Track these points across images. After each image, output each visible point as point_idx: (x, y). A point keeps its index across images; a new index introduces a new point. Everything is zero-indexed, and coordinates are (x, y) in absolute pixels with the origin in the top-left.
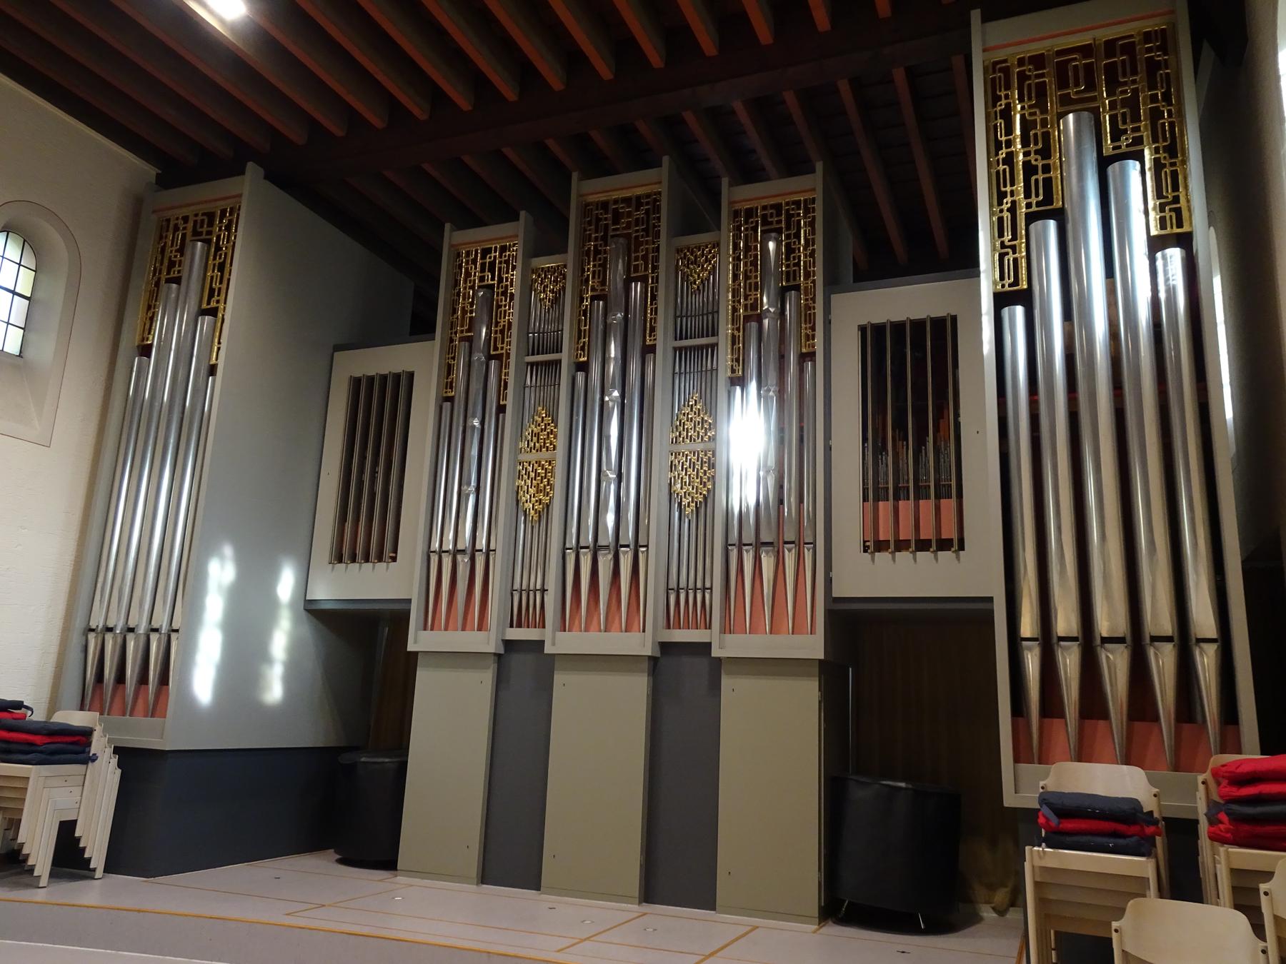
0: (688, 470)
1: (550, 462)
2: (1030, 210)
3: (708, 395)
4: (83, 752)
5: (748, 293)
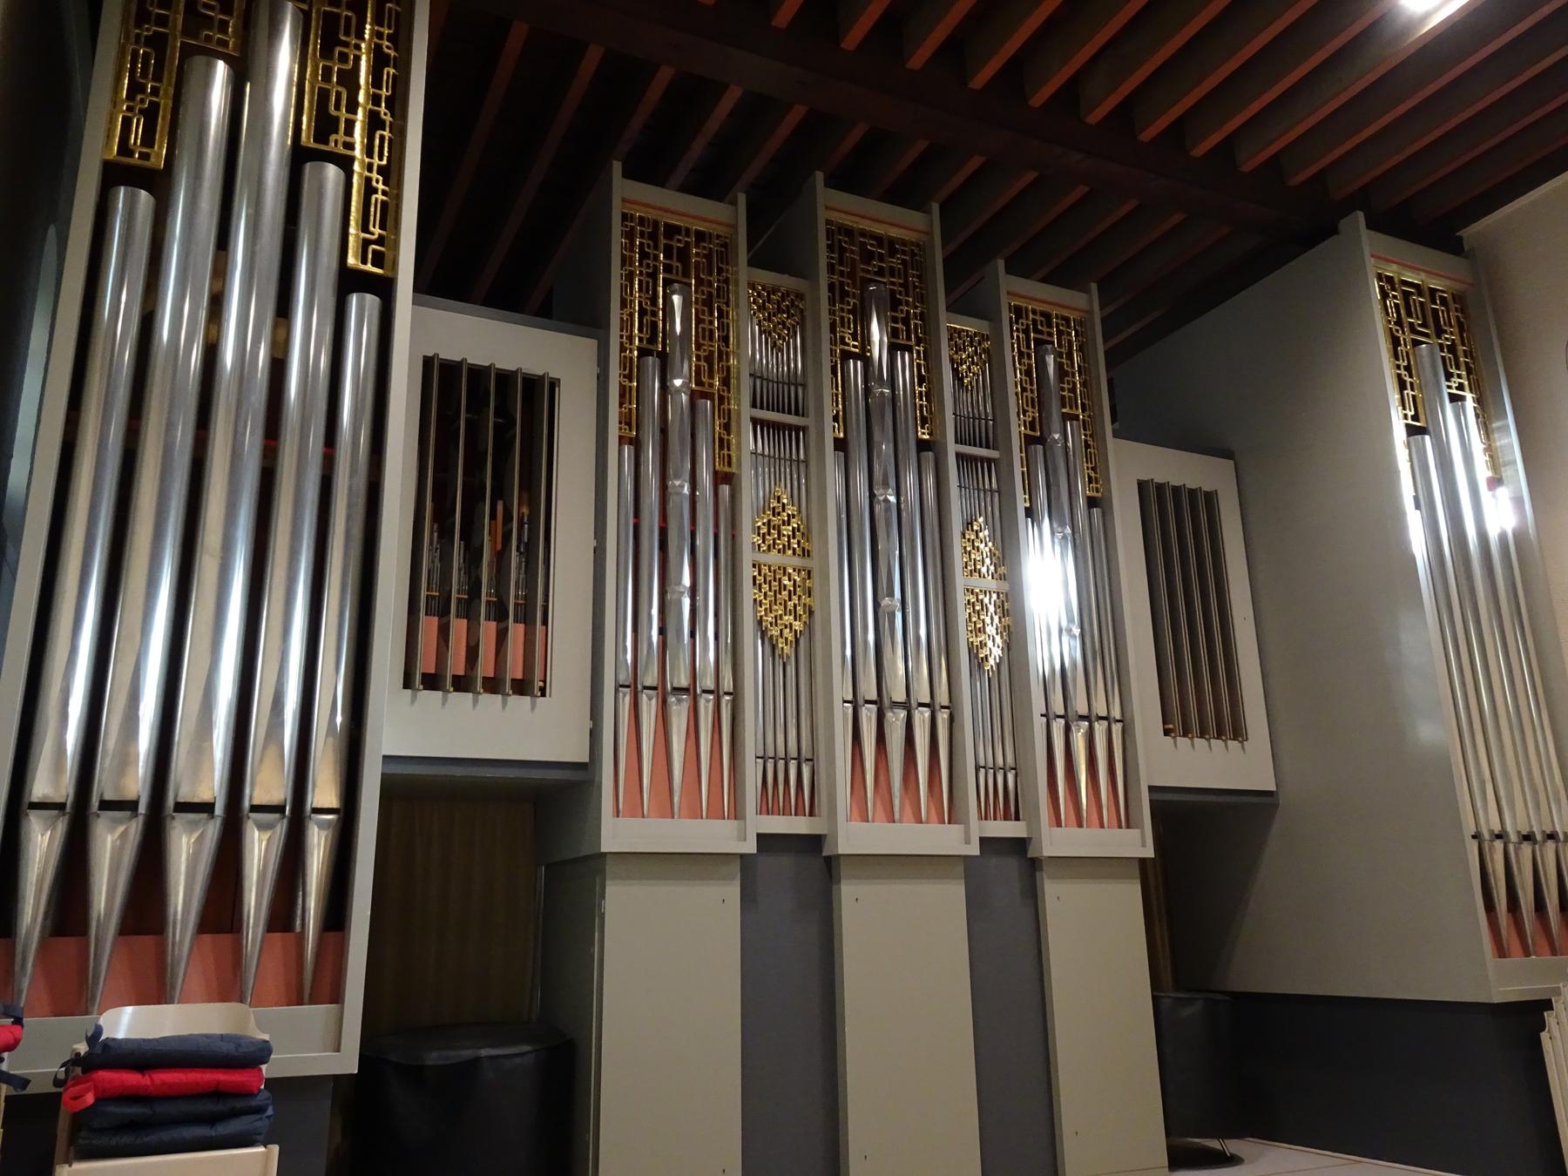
5: (701, 341)
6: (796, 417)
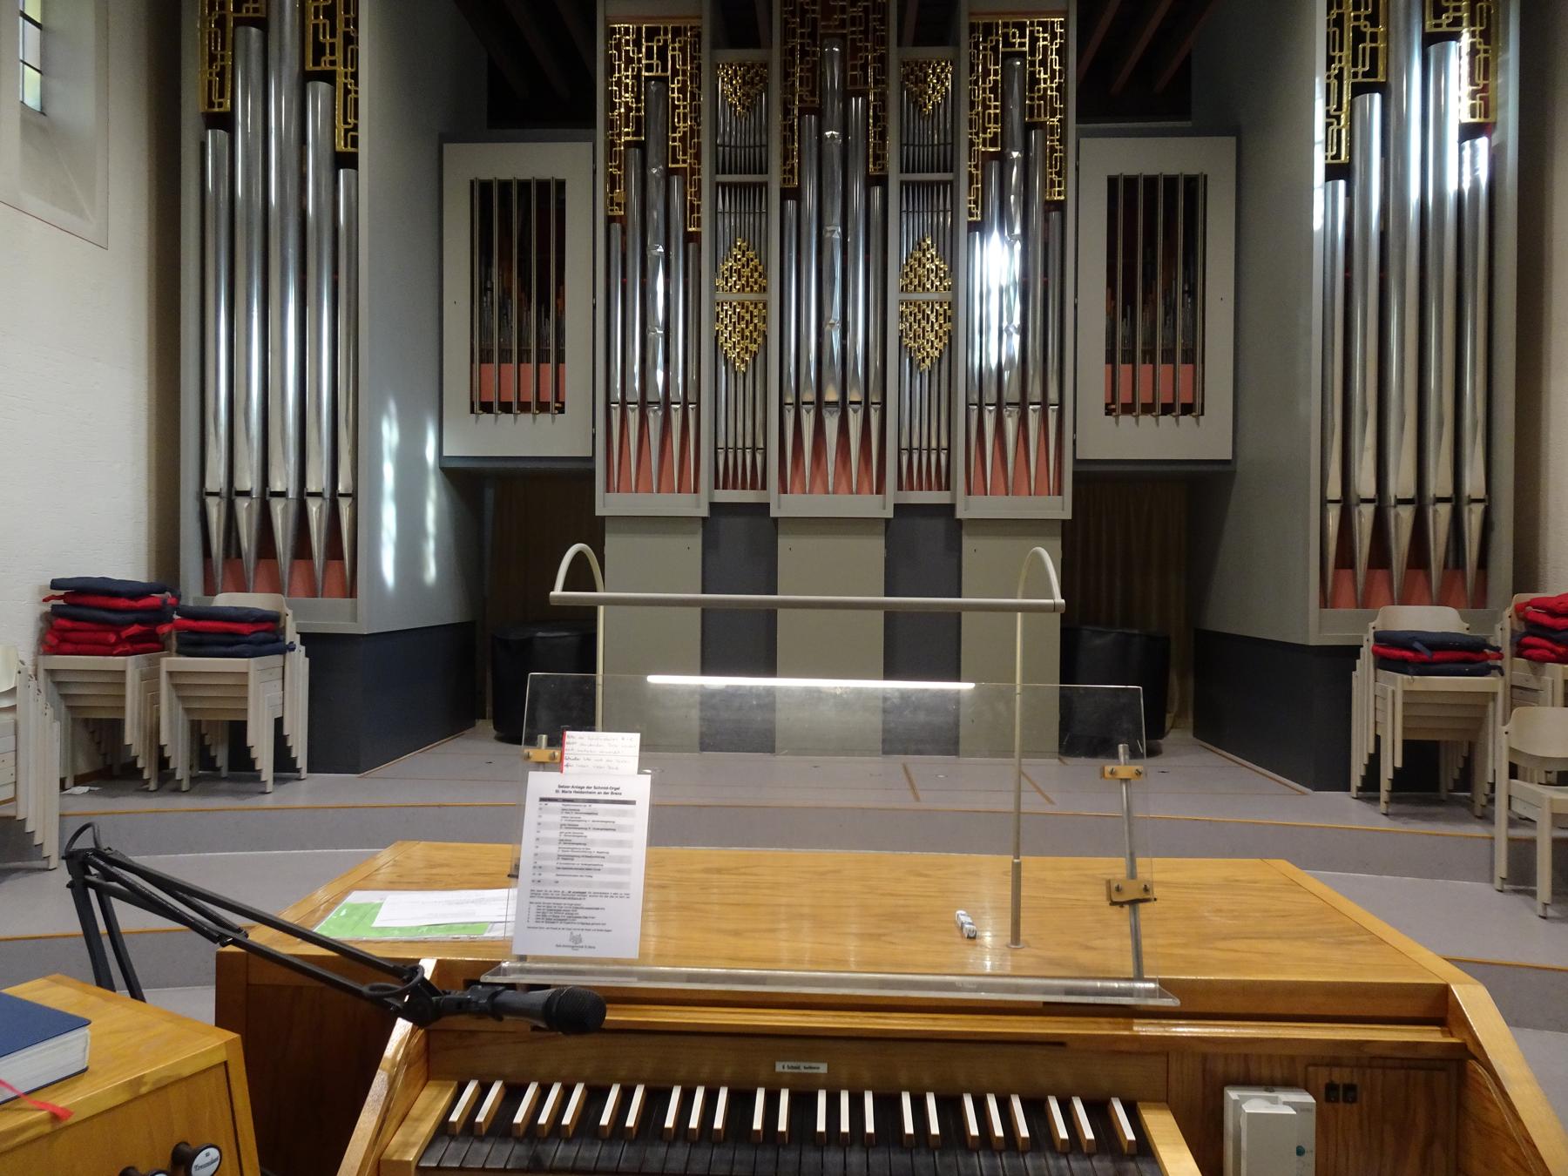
0: (922, 321)
1: (756, 304)
2: (1356, 80)
3: (941, 239)
4: (278, 640)
6: (760, 176)
